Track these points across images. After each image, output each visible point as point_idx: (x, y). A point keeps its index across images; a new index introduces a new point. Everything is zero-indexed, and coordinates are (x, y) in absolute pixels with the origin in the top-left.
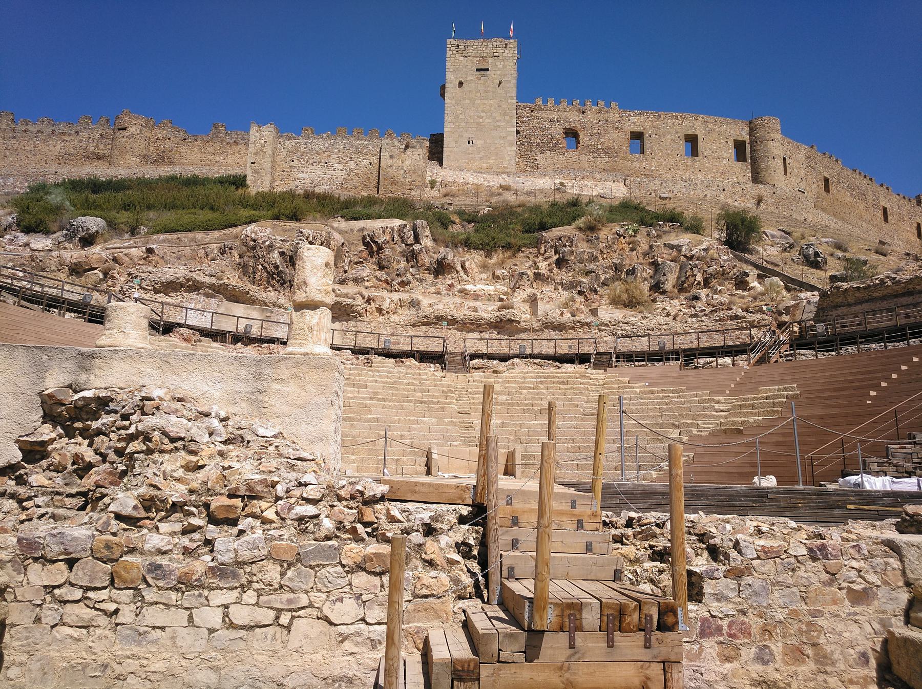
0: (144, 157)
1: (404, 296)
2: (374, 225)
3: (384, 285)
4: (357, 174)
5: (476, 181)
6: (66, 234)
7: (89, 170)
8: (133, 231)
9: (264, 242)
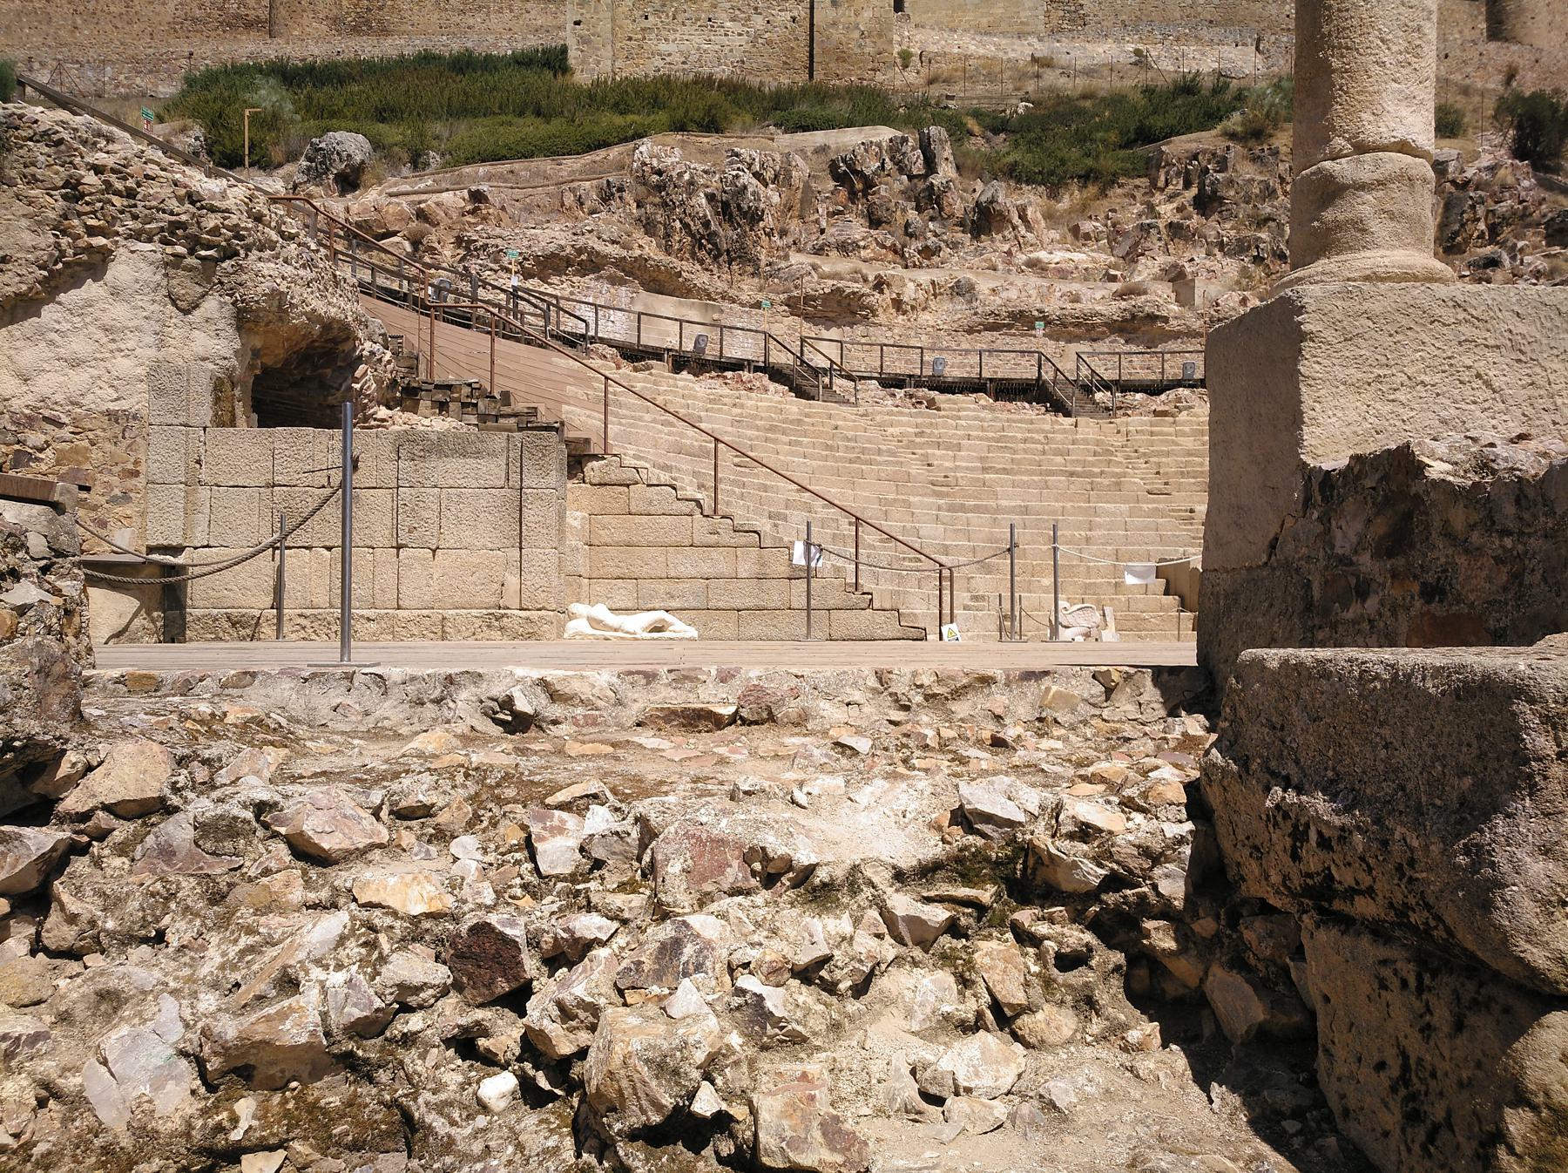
0: (335, 20)
1: (939, 276)
2: (848, 139)
3: (891, 256)
4: (769, 42)
5: (982, 51)
6: (309, 169)
7: (251, 47)
8: (417, 162)
9: (680, 175)
